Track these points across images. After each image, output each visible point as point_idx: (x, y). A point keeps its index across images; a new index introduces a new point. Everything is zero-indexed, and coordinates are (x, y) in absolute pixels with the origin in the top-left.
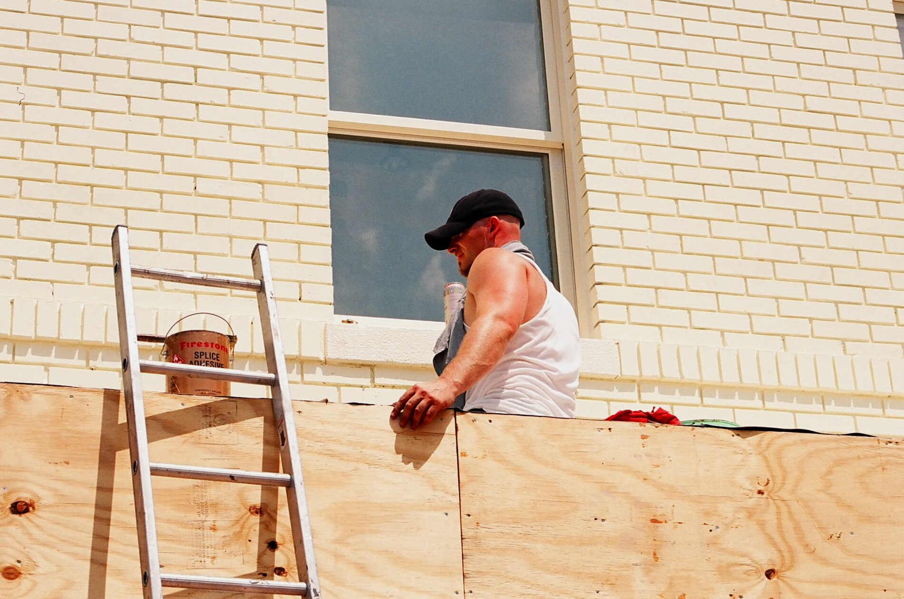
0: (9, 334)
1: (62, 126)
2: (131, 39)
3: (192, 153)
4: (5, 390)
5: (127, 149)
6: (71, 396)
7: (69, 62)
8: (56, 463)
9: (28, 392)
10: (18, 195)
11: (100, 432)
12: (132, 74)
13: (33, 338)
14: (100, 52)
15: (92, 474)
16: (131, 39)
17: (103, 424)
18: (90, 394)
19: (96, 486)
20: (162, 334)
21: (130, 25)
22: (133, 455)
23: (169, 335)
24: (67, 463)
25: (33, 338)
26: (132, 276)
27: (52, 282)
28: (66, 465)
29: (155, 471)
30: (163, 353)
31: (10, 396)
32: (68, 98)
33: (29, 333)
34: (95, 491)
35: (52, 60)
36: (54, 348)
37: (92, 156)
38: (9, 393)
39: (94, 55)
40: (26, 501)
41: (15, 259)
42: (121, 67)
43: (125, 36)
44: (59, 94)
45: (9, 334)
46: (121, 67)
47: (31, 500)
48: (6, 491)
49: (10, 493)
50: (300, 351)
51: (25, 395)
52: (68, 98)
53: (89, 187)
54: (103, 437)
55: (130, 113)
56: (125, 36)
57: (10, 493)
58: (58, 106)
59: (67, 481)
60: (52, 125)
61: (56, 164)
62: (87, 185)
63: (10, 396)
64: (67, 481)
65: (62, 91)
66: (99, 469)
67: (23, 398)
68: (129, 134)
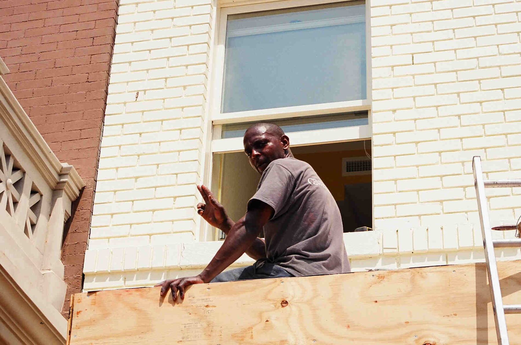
0: (442, 248)
1: (396, 88)
2: (500, 54)
3: (434, 71)
4: (411, 273)
5: (505, 122)
6: (454, 271)
7: (462, 76)
8: (448, 316)
9: (425, 272)
10: (440, 162)
11: (475, 292)
12: (503, 75)
13: (457, 248)
14: (481, 66)
15: (472, 320)
16: (500, 54)
17: (476, 287)
18: (466, 267)
19: (476, 328)
20: (515, 224)
21: (498, 46)
22: (94, 165)
23: (518, 224)
24: (455, 315)
25: (457, 248)
26: (485, 187)
27: (466, 212)
28: (455, 316)
29: (507, 311)
30: (516, 236)
31: (414, 276)
32: (464, 97)
33: (455, 246)
34: (476, 331)
35: (452, 76)
36: (472, 252)
37: (506, 139)
38: (413, 274)
39: (478, 68)
40: (431, 343)
41: (441, 202)
42: (496, 72)
43: (496, 52)
44: (459, 96)
45: (442, 248)
46: (496, 72)
47: (433, 342)
48: (416, 338)
49: (420, 338)
50: (118, 34)
51: (424, 274)
52: (464, 97)
53: (483, 149)
54: (477, 295)
55: (505, 99)
56: (496, 52)
57: (420, 338)
58: (458, 104)
59: (456, 327)
60: (456, 116)
61: (461, 139)
62: (482, 148)
63: (414, 276)
64: (456, 327)
65: (460, 94)
66: (477, 316)
67: (423, 277)
68: (505, 112)
